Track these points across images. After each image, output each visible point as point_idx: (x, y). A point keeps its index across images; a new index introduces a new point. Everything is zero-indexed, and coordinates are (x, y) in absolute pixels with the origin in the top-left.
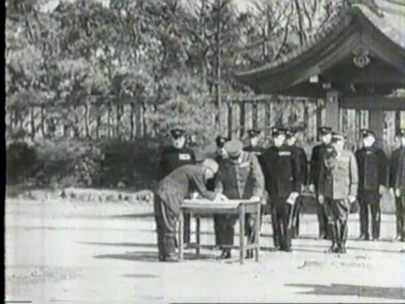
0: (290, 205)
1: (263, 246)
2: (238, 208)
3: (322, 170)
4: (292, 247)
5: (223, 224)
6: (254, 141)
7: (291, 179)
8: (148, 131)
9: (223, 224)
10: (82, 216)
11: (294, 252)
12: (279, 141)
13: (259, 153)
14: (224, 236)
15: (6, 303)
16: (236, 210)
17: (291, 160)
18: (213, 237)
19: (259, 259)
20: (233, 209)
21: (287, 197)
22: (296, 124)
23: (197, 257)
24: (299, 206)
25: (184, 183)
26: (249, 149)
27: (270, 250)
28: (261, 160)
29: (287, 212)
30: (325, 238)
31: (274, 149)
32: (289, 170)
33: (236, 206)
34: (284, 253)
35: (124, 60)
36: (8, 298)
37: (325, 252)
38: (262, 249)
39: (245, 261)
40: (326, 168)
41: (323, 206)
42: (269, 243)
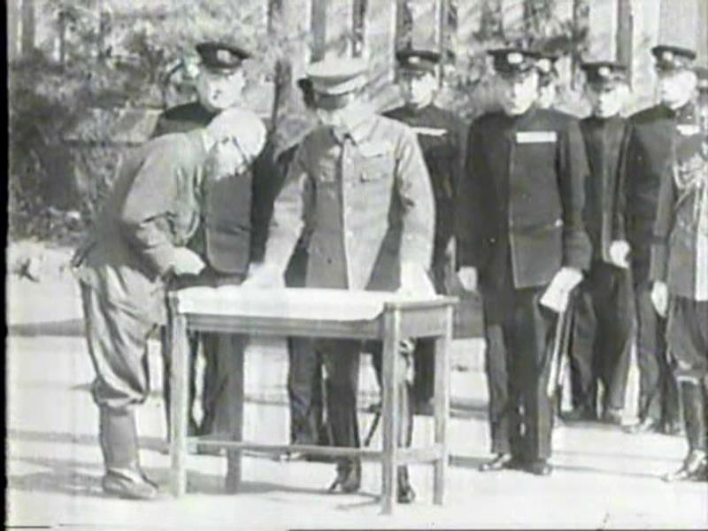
2: (381, 317)
3: (663, 194)
4: (552, 461)
5: (327, 376)
6: (424, 90)
7: (559, 223)
9: (327, 376)
11: (554, 472)
12: (524, 95)
15: (7, 530)
17: (559, 159)
21: (542, 290)
22: (548, 29)
23: (232, 484)
27: (479, 465)
28: (436, 157)
29: (541, 333)
30: (659, 427)
31: (496, 122)
32: (548, 196)
35: (605, 36)
36: (13, 519)
38: (455, 461)
39: (563, 439)
40: (675, 192)
41: (661, 322)
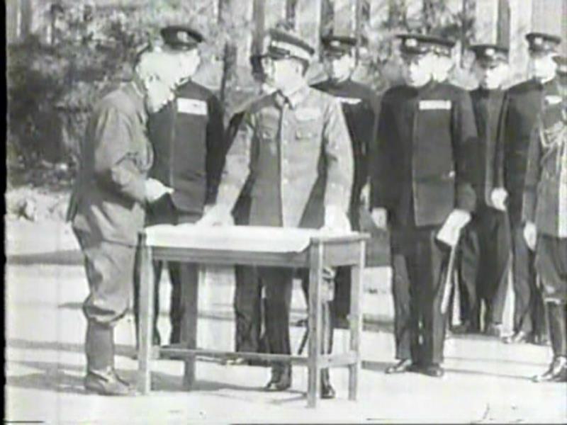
0: (444, 248)
1: (367, 359)
3: (532, 152)
5: (264, 298)
6: (343, 68)
7: (452, 174)
8: (36, 25)
9: (264, 298)
10: (177, 256)
11: (446, 376)
12: (428, 68)
13: (354, 101)
14: (262, 333)
17: (453, 122)
18: (230, 328)
20: (291, 255)
22: (443, 19)
23: (189, 383)
26: (328, 86)
27: (386, 368)
30: (530, 339)
31: (403, 93)
33: (300, 249)
37: (534, 380)
38: (365, 365)
40: (541, 152)
41: (531, 254)
42: (382, 346)
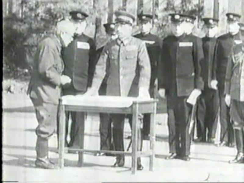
0: (190, 106)
1: (157, 153)
2: (131, 106)
3: (229, 65)
5: (113, 129)
6: (147, 28)
7: (193, 74)
9: (113, 129)
16: (130, 110)
17: (193, 52)
19: (154, 168)
23: (80, 163)
24: (199, 105)
25: (97, 136)
26: (141, 36)
30: (228, 145)
31: (172, 39)
34: (180, 161)
35: (209, 10)
38: (157, 156)
40: (233, 64)
41: (228, 108)
42: (164, 148)
